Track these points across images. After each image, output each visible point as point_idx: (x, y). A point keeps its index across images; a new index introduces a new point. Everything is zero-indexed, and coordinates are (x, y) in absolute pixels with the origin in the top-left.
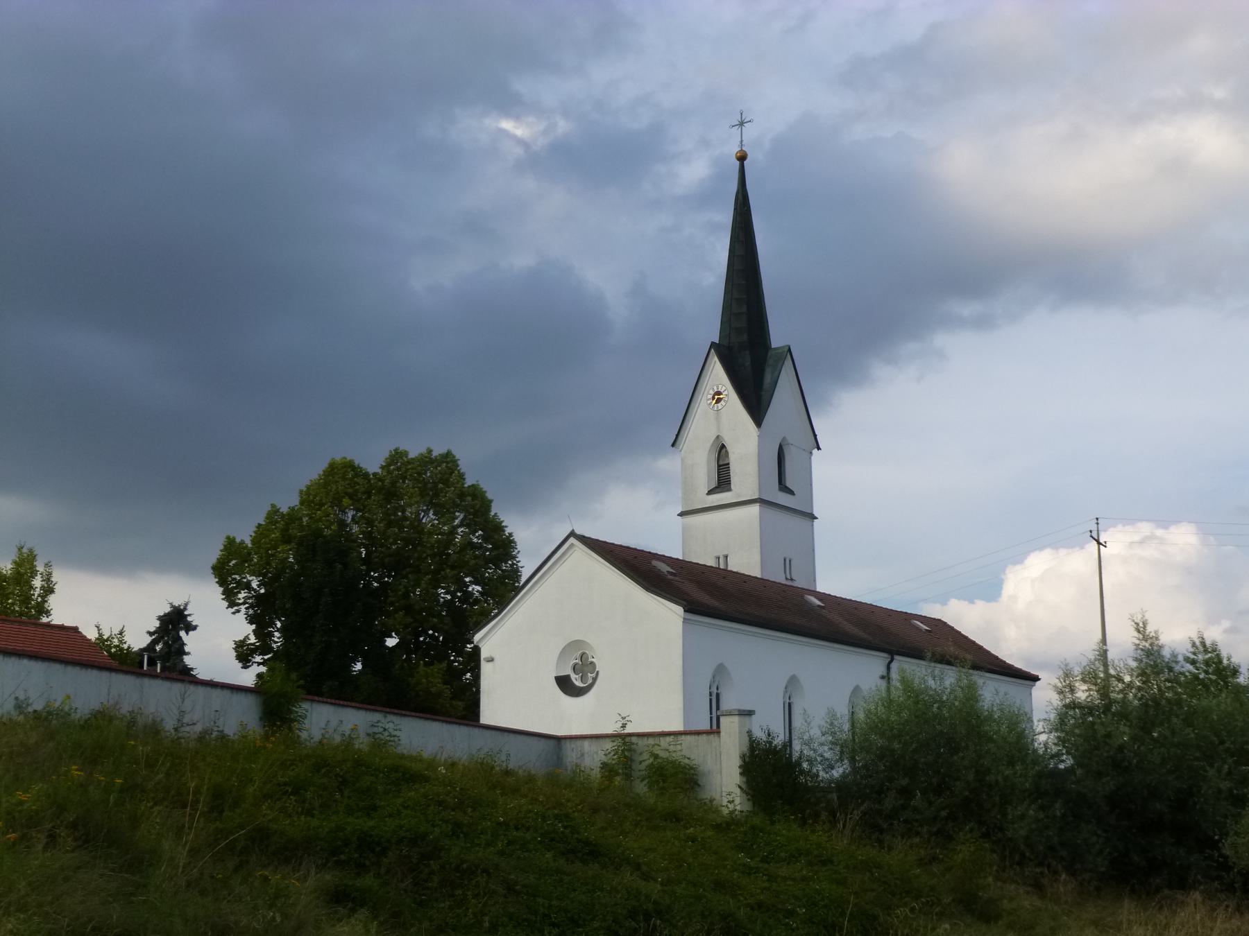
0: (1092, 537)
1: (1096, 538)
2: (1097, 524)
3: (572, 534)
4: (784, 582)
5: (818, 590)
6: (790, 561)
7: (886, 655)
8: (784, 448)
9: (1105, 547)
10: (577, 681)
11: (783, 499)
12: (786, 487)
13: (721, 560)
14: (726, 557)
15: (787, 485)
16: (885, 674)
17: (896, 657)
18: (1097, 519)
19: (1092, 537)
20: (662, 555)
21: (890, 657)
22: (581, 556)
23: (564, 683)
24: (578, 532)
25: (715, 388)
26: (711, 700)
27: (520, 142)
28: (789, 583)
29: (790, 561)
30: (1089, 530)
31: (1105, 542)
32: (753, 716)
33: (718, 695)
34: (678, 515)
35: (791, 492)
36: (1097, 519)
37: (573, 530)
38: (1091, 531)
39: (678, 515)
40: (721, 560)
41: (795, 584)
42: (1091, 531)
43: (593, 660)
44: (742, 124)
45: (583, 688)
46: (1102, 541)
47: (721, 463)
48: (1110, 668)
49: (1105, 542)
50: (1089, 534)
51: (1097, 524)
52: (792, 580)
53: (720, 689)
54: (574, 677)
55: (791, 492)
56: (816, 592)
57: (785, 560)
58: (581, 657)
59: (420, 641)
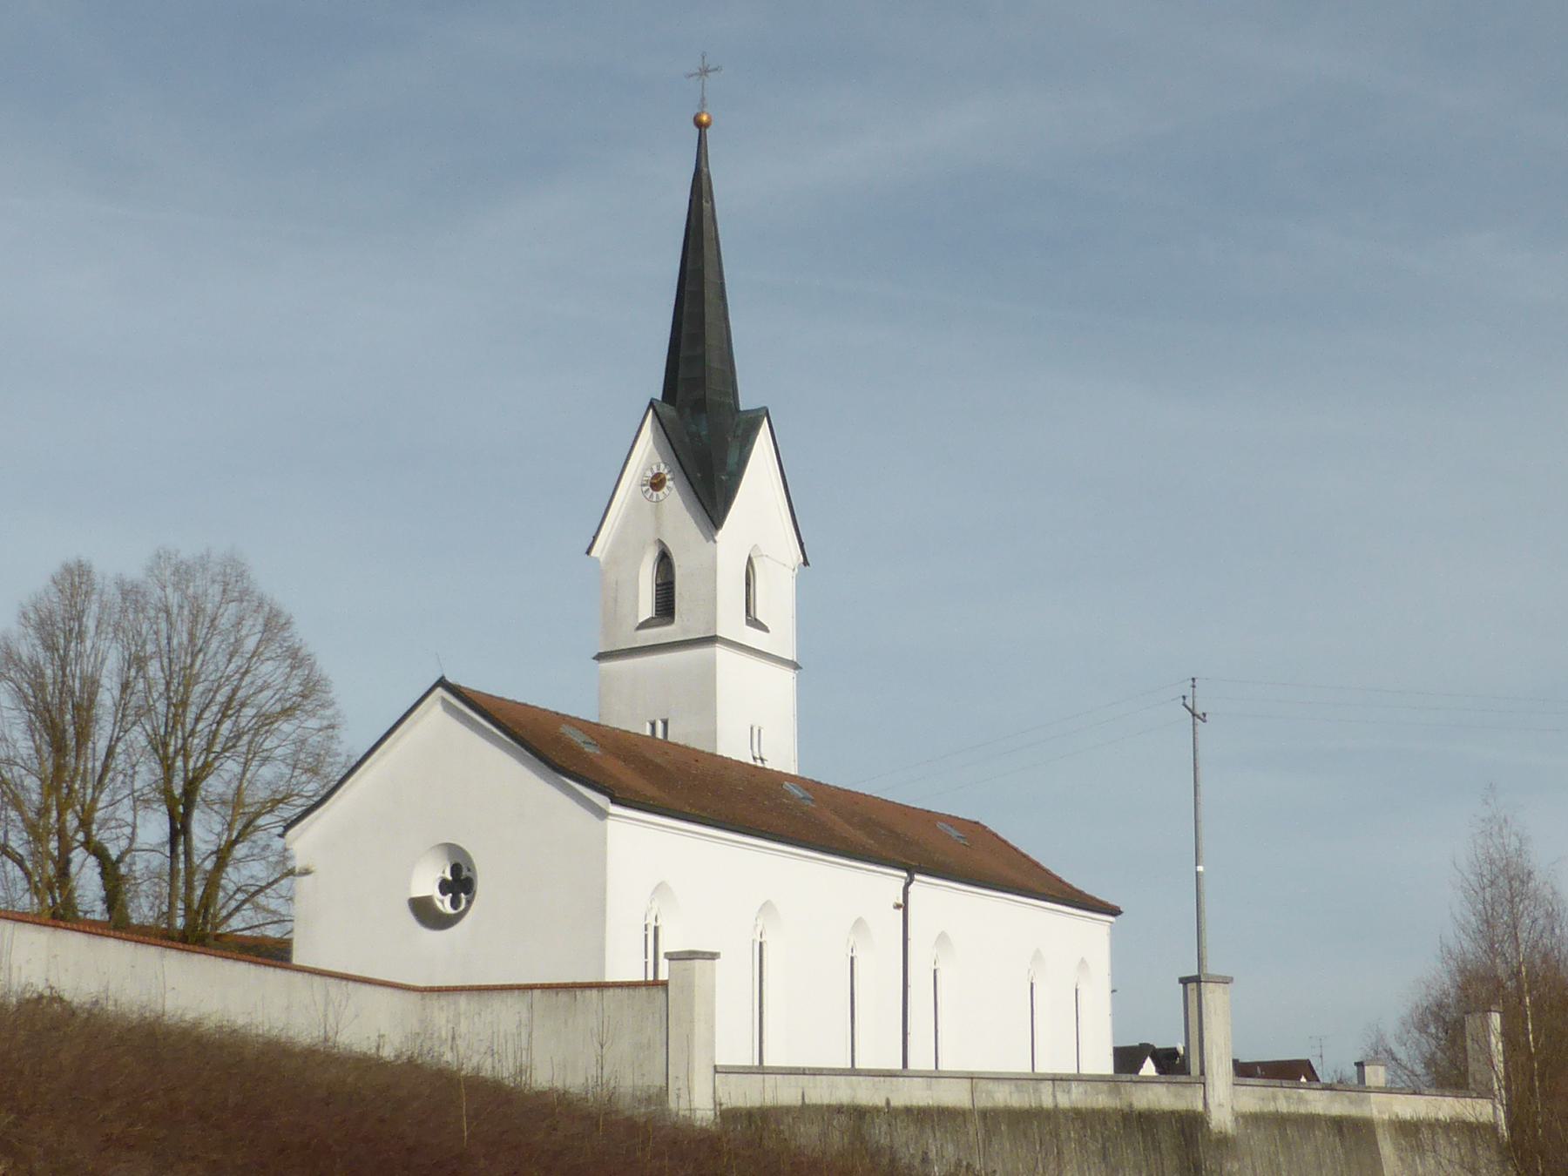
0: (1186, 706)
1: (1191, 707)
2: (1194, 686)
3: (442, 683)
4: (751, 762)
5: (719, 753)
6: (759, 731)
8: (755, 561)
9: (1205, 721)
10: (444, 905)
11: (752, 637)
12: (756, 620)
13: (659, 726)
14: (665, 723)
15: (758, 617)
16: (901, 901)
17: (917, 877)
18: (1193, 679)
19: (1186, 706)
20: (575, 718)
22: (435, 716)
23: (423, 911)
24: (450, 679)
25: (655, 468)
26: (646, 936)
27: (1404, 1140)
28: (759, 764)
29: (759, 731)
30: (1181, 695)
31: (1204, 715)
32: (717, 960)
33: (656, 929)
34: (594, 658)
35: (763, 628)
36: (1193, 679)
37: (443, 677)
38: (1184, 697)
39: (594, 658)
40: (659, 726)
41: (768, 765)
42: (1184, 697)
44: (704, 72)
45: (455, 915)
46: (1199, 712)
48: (1499, 1030)
49: (1204, 715)
50: (1181, 700)
51: (1194, 686)
52: (762, 760)
53: (659, 920)
55: (763, 628)
56: (716, 756)
57: (752, 729)
58: (1455, 864)
59: (1204, 869)
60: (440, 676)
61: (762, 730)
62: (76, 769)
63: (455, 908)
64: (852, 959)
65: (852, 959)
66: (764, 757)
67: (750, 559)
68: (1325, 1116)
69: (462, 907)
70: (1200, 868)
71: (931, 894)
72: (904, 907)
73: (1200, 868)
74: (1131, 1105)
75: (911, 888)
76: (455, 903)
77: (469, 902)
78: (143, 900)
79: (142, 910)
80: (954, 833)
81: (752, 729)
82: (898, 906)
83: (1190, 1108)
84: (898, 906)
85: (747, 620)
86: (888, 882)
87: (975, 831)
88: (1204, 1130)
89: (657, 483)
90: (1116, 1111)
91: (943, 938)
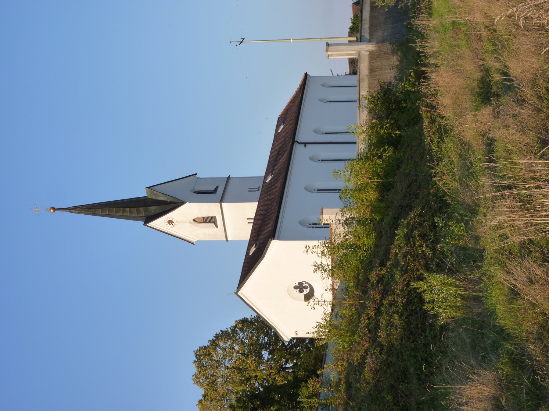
6: (250, 189)
9: (244, 38)
10: (306, 291)
16: (304, 145)
17: (296, 139)
18: (231, 42)
22: (244, 291)
24: (235, 290)
26: (316, 227)
29: (250, 189)
31: (242, 38)
34: (217, 228)
36: (231, 42)
46: (241, 40)
47: (203, 221)
57: (249, 191)
60: (234, 294)
61: (250, 188)
62: (510, 242)
63: (308, 287)
64: (325, 133)
65: (325, 133)
66: (258, 187)
67: (196, 192)
68: (370, 12)
69: (307, 285)
70: (292, 41)
71: (301, 136)
72: (305, 144)
73: (292, 41)
74: (367, 75)
75: (299, 141)
76: (306, 288)
77: (306, 283)
78: (511, 10)
79: (356, 83)
80: (282, 127)
81: (249, 191)
82: (305, 146)
83: (368, 56)
84: (305, 146)
85: (215, 193)
86: (298, 150)
87: (282, 120)
88: (375, 52)
89: (170, 222)
90: (369, 80)
91: (316, 131)
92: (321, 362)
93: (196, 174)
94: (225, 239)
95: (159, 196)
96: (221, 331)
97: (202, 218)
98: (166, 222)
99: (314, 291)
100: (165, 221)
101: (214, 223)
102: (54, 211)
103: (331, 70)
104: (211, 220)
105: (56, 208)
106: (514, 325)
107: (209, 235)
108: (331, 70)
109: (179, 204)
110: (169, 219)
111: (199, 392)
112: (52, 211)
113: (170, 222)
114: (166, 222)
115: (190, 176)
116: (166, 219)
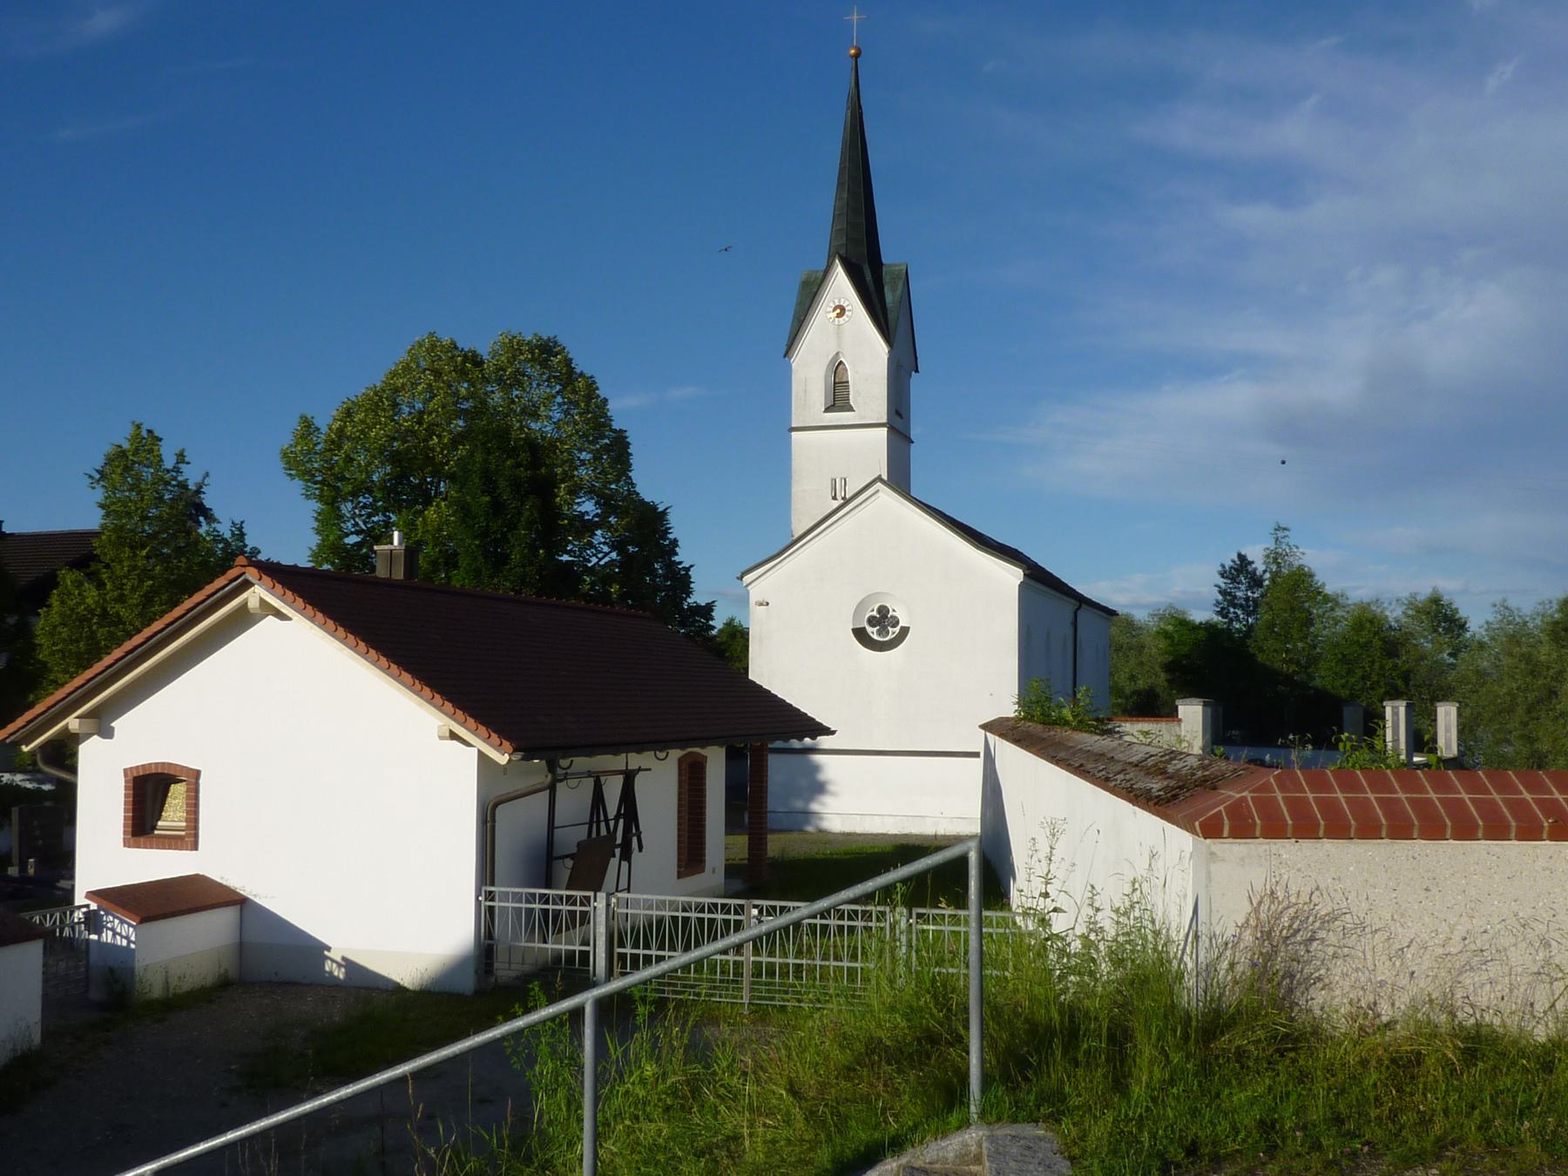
7: (1073, 601)
10: (873, 632)
21: (1078, 604)
23: (860, 634)
43: (894, 614)
47: (837, 380)
54: (869, 629)
92: (1130, 624)
93: (917, 371)
94: (794, 425)
95: (894, 290)
96: (606, 400)
97: (844, 380)
98: (839, 301)
99: (281, 620)
100: (843, 300)
101: (832, 406)
102: (852, 56)
103: (650, 770)
104: (838, 398)
105: (858, 60)
106: (1149, 1045)
107: (806, 391)
108: (650, 770)
109: (886, 332)
110: (847, 309)
111: (483, 342)
112: (853, 51)
113: (841, 311)
114: (839, 301)
115: (916, 358)
116: (847, 303)
